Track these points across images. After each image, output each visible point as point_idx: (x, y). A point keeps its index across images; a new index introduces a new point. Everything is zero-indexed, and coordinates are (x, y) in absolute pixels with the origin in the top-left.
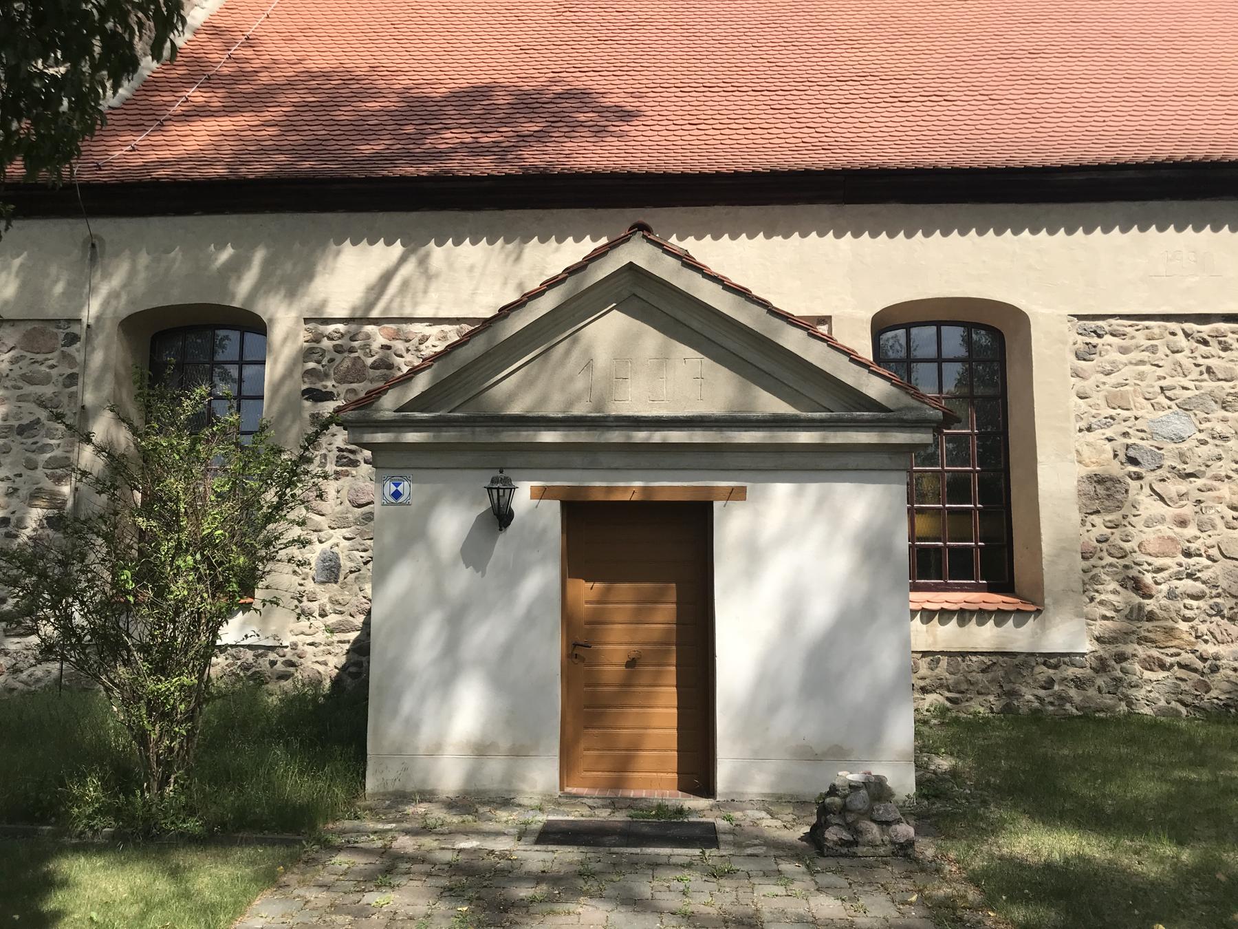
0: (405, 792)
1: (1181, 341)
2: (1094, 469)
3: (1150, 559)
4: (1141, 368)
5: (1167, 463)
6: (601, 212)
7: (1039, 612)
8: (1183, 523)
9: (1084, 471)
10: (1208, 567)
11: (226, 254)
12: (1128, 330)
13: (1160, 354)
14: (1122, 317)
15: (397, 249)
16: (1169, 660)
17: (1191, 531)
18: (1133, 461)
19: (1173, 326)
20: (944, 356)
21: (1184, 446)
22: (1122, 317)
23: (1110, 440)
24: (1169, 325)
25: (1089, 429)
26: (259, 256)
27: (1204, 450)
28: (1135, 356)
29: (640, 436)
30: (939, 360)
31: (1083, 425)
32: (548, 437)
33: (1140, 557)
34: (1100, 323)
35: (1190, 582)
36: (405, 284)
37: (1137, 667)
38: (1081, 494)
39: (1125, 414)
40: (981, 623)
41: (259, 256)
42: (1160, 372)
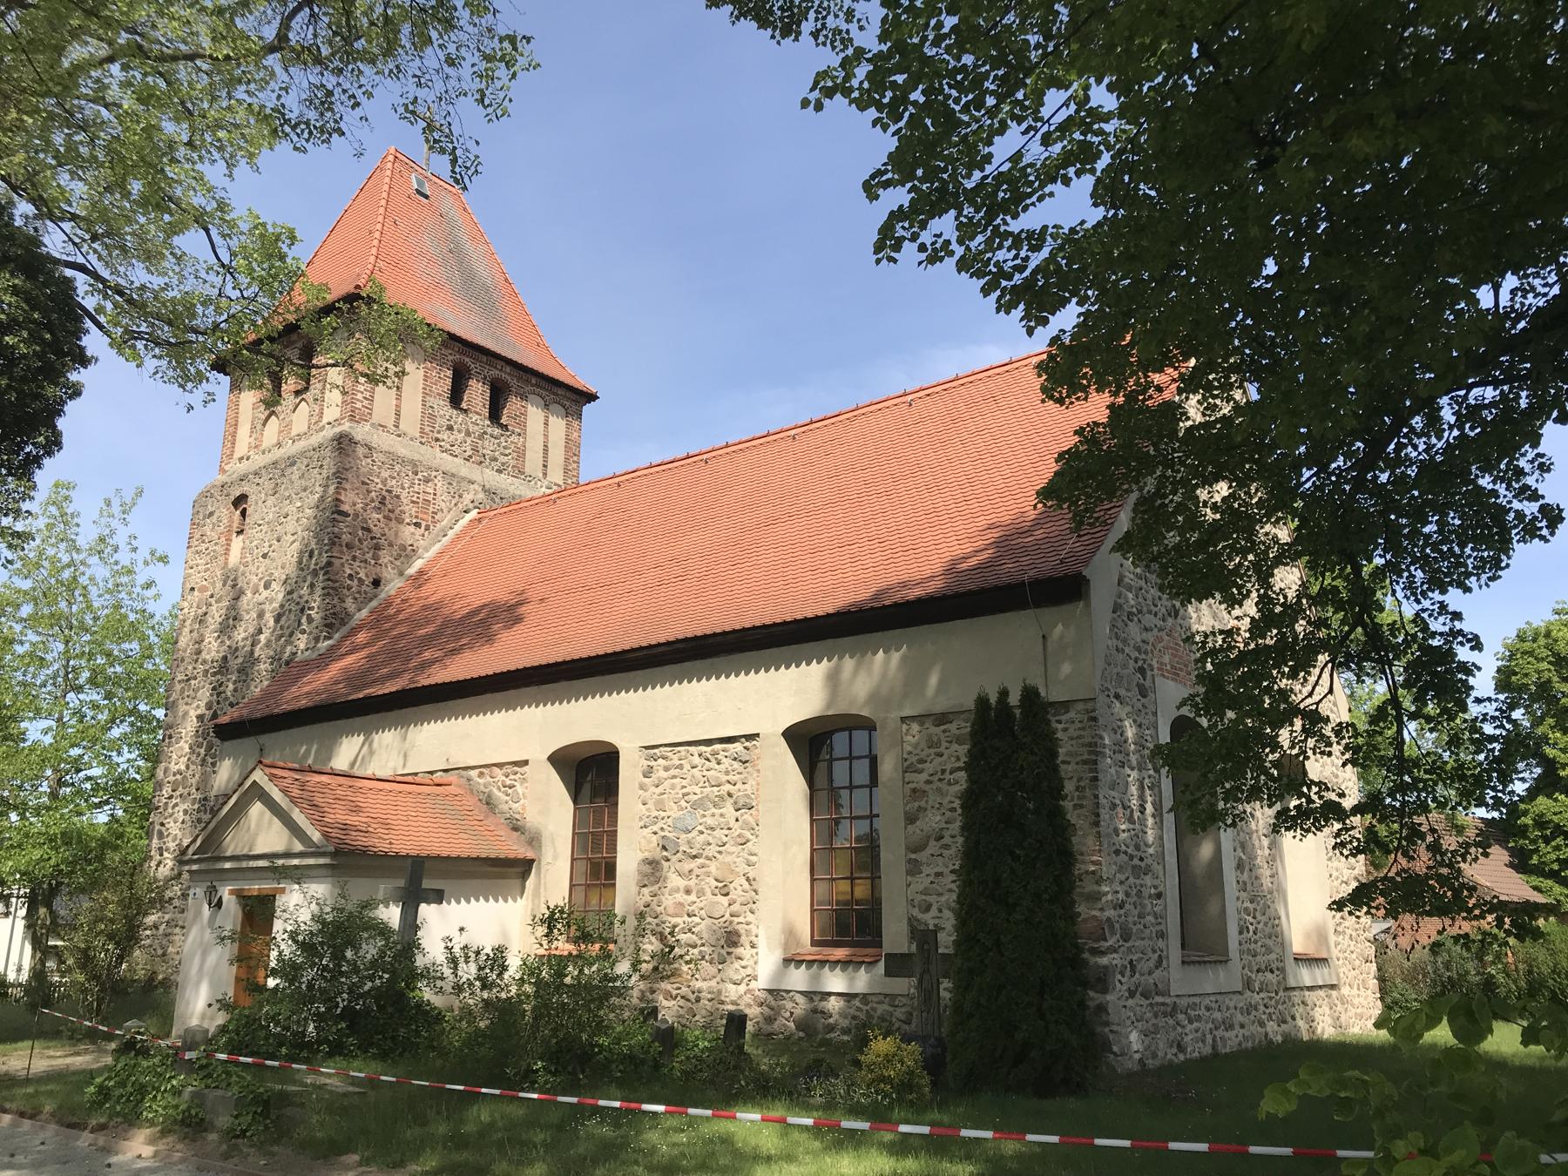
0: (856, 1149)
1: (696, 760)
2: (647, 854)
3: (670, 919)
4: (674, 781)
5: (682, 848)
6: (608, 677)
7: (1226, 962)
8: (688, 892)
9: (641, 856)
10: (698, 924)
11: (304, 748)
12: (670, 754)
13: (685, 770)
14: (666, 745)
15: (362, 737)
16: (674, 992)
17: (693, 897)
18: (664, 848)
19: (692, 749)
20: (854, 754)
21: (690, 835)
22: (666, 745)
23: (655, 833)
24: (690, 748)
25: (646, 827)
26: (315, 747)
27: (701, 838)
28: (673, 772)
29: (244, 864)
30: (851, 758)
31: (642, 824)
32: (228, 865)
33: (665, 918)
34: (656, 751)
35: (689, 935)
36: (363, 759)
37: (661, 998)
38: (640, 872)
39: (663, 814)
40: (797, 967)
41: (315, 747)
42: (684, 783)
